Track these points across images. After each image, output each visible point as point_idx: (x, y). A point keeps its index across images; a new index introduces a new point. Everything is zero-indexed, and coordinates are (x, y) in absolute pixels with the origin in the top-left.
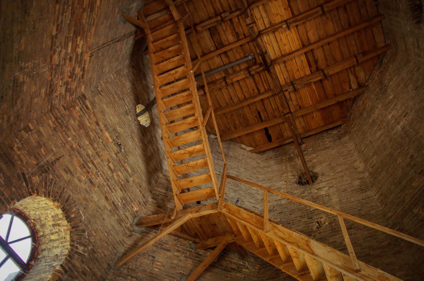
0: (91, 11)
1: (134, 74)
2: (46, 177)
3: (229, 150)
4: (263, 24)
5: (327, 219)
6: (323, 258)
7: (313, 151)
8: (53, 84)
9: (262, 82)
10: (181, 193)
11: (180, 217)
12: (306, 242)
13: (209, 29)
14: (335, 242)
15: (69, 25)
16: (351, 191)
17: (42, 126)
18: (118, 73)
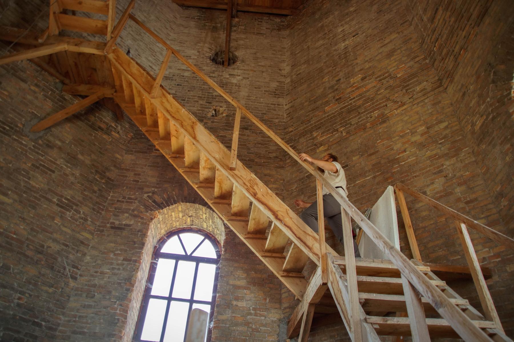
5: (226, 111)
6: (203, 146)
10: (61, 13)
11: (51, 44)
12: (192, 124)
14: (225, 137)
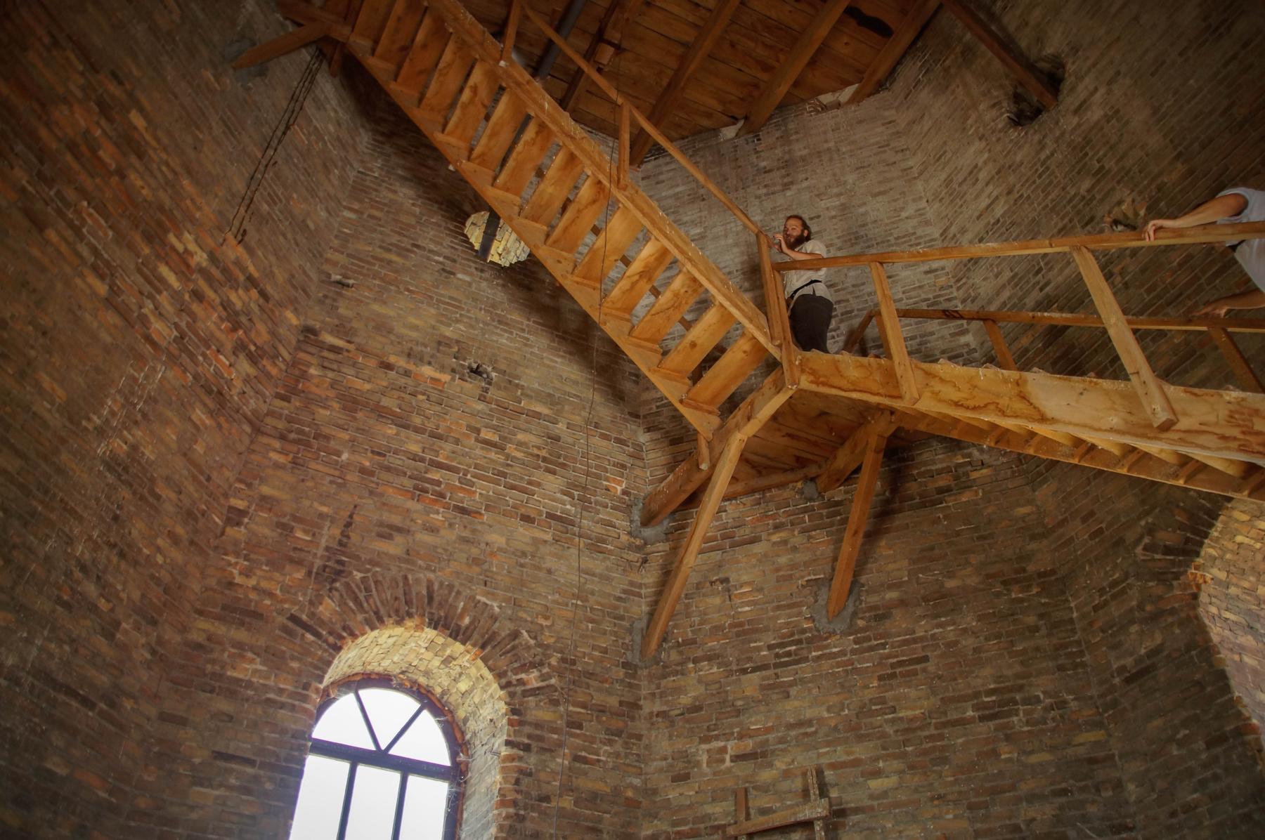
0: (140, 156)
2: (347, 585)
6: (1070, 423)
8: (207, 380)
16: (1181, 54)
17: (262, 480)
18: (359, 191)
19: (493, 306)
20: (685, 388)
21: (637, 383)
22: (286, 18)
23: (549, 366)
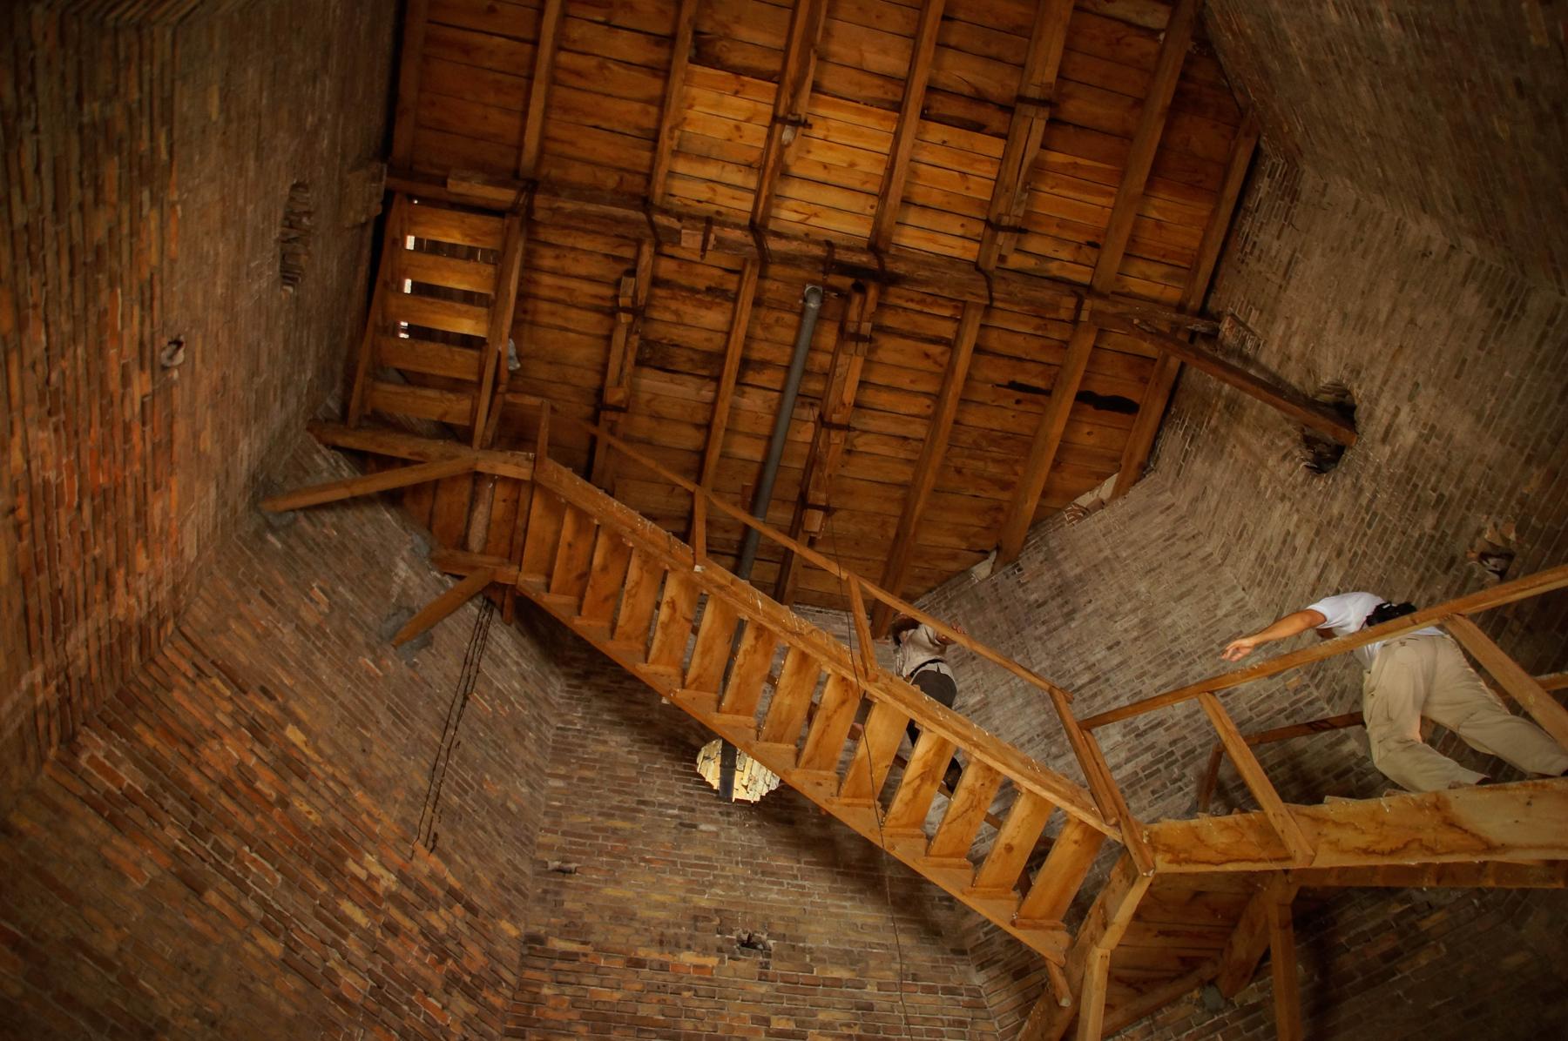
0: (302, 777)
1: (605, 692)
3: (1058, 564)
4: (738, 193)
5: (1501, 522)
7: (1265, 315)
9: (921, 312)
13: (640, 363)
15: (291, 880)
18: (562, 751)
19: (752, 855)
20: (1014, 905)
21: (951, 908)
22: (444, 574)
23: (837, 915)
